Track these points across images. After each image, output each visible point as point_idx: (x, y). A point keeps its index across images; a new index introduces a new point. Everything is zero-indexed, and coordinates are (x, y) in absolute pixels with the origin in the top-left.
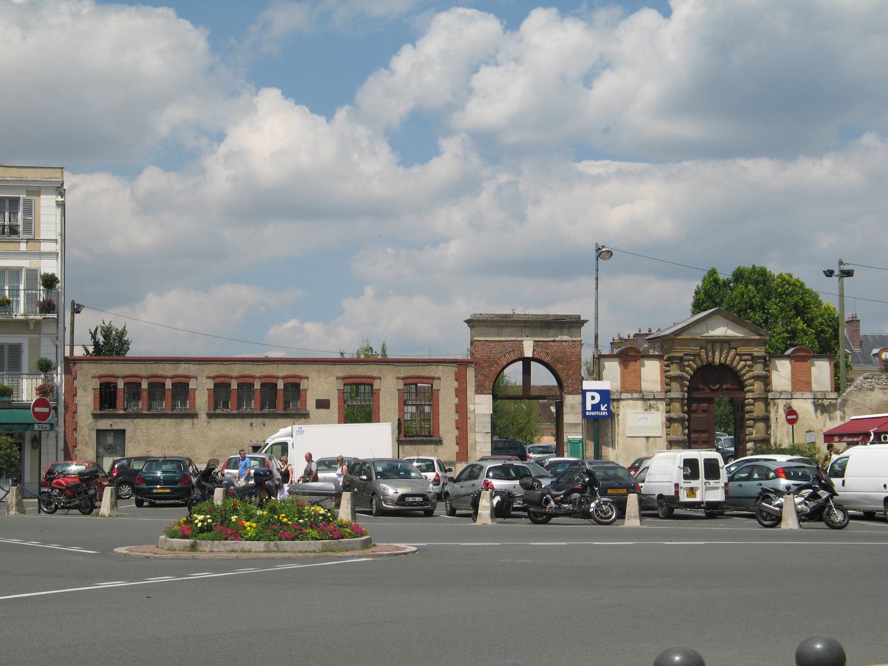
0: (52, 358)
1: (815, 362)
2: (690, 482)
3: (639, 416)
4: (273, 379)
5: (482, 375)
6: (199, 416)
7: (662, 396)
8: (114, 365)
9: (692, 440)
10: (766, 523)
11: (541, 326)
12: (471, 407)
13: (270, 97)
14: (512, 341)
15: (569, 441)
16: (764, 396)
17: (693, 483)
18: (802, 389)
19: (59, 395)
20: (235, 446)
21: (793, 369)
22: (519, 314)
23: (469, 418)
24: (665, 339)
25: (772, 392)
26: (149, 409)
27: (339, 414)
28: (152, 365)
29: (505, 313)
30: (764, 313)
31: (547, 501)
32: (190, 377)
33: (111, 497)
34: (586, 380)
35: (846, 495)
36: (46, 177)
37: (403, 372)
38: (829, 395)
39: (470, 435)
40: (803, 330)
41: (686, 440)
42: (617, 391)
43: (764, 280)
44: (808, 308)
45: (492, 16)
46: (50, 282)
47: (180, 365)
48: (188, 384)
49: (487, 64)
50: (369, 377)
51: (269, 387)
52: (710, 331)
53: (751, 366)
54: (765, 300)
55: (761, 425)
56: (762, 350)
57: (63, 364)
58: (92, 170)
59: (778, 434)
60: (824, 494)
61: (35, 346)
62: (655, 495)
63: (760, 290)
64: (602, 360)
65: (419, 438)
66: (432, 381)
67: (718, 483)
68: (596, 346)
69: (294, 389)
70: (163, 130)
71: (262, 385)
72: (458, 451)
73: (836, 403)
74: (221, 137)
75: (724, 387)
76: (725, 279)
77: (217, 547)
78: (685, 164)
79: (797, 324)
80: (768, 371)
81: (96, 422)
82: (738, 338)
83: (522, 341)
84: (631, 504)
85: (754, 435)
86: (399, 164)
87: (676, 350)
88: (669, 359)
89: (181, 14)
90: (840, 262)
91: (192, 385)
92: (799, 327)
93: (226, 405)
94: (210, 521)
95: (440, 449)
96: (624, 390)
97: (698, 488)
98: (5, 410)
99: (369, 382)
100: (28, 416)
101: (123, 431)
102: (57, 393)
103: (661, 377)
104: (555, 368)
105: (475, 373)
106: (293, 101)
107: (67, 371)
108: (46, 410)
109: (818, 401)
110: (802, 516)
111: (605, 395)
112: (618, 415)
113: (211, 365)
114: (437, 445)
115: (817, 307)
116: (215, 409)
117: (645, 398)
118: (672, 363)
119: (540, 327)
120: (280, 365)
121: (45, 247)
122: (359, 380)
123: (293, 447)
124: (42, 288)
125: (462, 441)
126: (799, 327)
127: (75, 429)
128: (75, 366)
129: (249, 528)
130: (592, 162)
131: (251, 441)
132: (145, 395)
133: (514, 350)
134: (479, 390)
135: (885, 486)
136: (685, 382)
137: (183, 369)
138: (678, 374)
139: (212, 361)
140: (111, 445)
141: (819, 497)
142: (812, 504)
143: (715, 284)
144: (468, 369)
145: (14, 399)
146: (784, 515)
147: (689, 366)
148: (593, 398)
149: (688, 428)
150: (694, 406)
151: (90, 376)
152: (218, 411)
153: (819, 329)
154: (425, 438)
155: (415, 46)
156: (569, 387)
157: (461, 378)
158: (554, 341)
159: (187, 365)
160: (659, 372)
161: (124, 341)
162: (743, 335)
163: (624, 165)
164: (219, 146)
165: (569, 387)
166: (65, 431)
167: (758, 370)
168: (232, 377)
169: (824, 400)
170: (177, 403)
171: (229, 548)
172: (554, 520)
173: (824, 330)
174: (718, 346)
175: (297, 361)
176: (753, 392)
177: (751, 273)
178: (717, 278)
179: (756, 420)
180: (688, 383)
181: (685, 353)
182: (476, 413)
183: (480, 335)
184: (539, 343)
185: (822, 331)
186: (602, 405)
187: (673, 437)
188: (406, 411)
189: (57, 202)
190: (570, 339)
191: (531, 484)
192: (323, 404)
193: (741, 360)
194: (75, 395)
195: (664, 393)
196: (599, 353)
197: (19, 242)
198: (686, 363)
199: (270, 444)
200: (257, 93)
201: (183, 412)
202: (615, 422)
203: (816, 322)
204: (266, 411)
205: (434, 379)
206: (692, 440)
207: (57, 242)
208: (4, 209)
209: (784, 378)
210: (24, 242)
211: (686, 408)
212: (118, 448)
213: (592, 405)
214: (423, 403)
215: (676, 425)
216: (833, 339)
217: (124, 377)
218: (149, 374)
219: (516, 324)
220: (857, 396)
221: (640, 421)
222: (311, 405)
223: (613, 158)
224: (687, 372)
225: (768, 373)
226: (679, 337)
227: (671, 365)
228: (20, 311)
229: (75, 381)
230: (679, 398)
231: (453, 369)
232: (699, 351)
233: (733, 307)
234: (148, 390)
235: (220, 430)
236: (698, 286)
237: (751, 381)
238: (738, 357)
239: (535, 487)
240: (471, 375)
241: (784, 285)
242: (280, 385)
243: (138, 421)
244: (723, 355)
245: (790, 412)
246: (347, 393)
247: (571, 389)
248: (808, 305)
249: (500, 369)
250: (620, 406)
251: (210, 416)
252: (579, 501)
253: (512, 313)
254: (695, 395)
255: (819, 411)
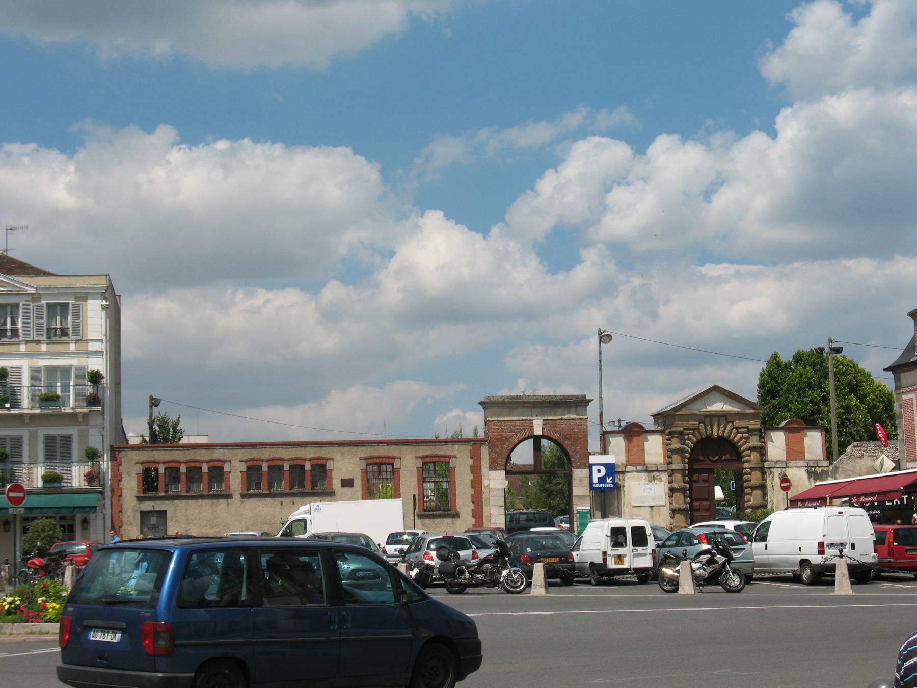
0: (98, 446)
1: (808, 433)
2: (618, 550)
3: (644, 487)
4: (301, 461)
5: (495, 452)
6: (234, 497)
7: (664, 467)
8: (155, 452)
9: (694, 508)
10: (665, 588)
11: (549, 406)
12: (485, 482)
13: (434, 219)
14: (522, 420)
15: (578, 512)
16: (761, 465)
17: (621, 551)
18: (796, 458)
19: (106, 480)
20: (267, 524)
21: (787, 439)
22: (528, 396)
23: (484, 493)
24: (666, 415)
25: (768, 461)
26: (188, 491)
27: (363, 492)
28: (189, 451)
29: (516, 395)
30: (821, 391)
31: (461, 572)
32: (224, 461)
33: (72, 576)
34: (594, 455)
35: (768, 558)
36: (92, 284)
37: (421, 451)
38: (820, 463)
39: (485, 508)
40: (856, 405)
41: (687, 508)
42: (622, 464)
43: (821, 362)
44: (860, 386)
45: (623, 143)
46: (95, 378)
47: (216, 451)
48: (222, 468)
49: (619, 184)
50: (389, 457)
51: (297, 468)
52: (708, 407)
53: (747, 438)
54: (822, 380)
55: (758, 493)
56: (757, 423)
57: (109, 452)
58: (283, 287)
59: (775, 501)
60: (721, 559)
61: (84, 436)
62: (587, 562)
63: (817, 370)
64: (607, 436)
65: (438, 512)
66: (448, 459)
67: (646, 549)
68: (601, 423)
69: (321, 470)
70: (343, 250)
71: (165, 469)
72: (474, 523)
73: (828, 470)
74: (391, 254)
75: (723, 458)
76: (786, 362)
77: (17, 629)
78: (796, 265)
79: (850, 400)
80: (764, 442)
81: (140, 504)
82: (734, 412)
83: (532, 420)
84: (537, 573)
85: (752, 502)
86: (546, 273)
87: (677, 425)
88: (670, 433)
89: (356, 152)
90: (830, 340)
91: (227, 468)
92: (853, 403)
93: (258, 486)
94: (18, 603)
95: (458, 522)
96: (629, 463)
97: (625, 556)
98: (55, 495)
99: (389, 461)
100: (77, 500)
101: (165, 512)
102: (104, 479)
103: (664, 450)
104: (564, 445)
105: (489, 450)
106: (454, 221)
107: (113, 458)
108: (21, 495)
109: (811, 469)
110: (700, 581)
111: (611, 469)
112: (624, 486)
113: (243, 450)
114: (454, 518)
115: (869, 385)
116: (248, 490)
117: (650, 471)
118: (673, 437)
119: (548, 407)
120: (307, 448)
121: (92, 347)
122: (381, 460)
123: (311, 524)
124: (89, 384)
125: (478, 514)
126: (853, 403)
127: (121, 511)
128: (120, 454)
129: (51, 610)
130: (714, 266)
131: (281, 519)
132: (183, 478)
133: (524, 429)
134: (493, 466)
135: (800, 549)
136: (686, 454)
137: (218, 454)
138: (679, 447)
139: (244, 446)
140: (154, 525)
141: (716, 562)
142: (709, 569)
143: (778, 366)
144: (482, 447)
145: (65, 485)
146: (681, 580)
147: (689, 439)
148: (599, 471)
149: (690, 497)
150: (695, 476)
151: (134, 462)
152: (251, 492)
153: (871, 404)
154: (442, 512)
155: (557, 171)
156: (576, 462)
157: (475, 456)
158: (561, 419)
159: (221, 450)
160: (662, 446)
161: (177, 430)
162: (739, 410)
163: (742, 268)
164: (390, 262)
165: (576, 462)
166: (111, 513)
167: (754, 441)
168: (263, 460)
169: (817, 468)
170: (213, 485)
171: (28, 630)
172: (468, 590)
173: (876, 405)
174: (715, 420)
175: (323, 444)
176: (750, 462)
177: (809, 356)
178: (779, 361)
179: (753, 488)
180: (688, 455)
181: (685, 427)
182: (490, 487)
183: (492, 416)
184: (548, 422)
185: (874, 407)
186: (607, 478)
187: (675, 506)
188: (425, 488)
189: (102, 305)
190: (577, 417)
191: (447, 555)
192: (347, 483)
193: (738, 433)
194: (120, 480)
195: (666, 465)
196: (604, 430)
197: (69, 343)
198: (686, 437)
199: (290, 521)
200: (422, 215)
201: (218, 493)
202: (620, 493)
203: (868, 398)
204: (295, 490)
205: (450, 457)
206: (694, 508)
207: (102, 342)
208: (56, 314)
209: (779, 448)
210: (73, 343)
211: (687, 478)
212: (161, 528)
213: (598, 478)
214: (441, 480)
215: (678, 494)
216: (884, 413)
217: (164, 463)
218: (187, 459)
219: (526, 405)
220: (847, 464)
221: (644, 491)
222: (336, 483)
223: (732, 261)
224: (687, 445)
225: (764, 444)
226: (678, 413)
227: (672, 439)
228: (71, 404)
229: (120, 467)
230: (681, 470)
231: (468, 448)
232: (698, 425)
233: (793, 386)
234: (186, 474)
235: (253, 509)
236: (763, 369)
237: (747, 452)
238: (735, 430)
239: (451, 558)
240: (485, 453)
241: (838, 366)
242: (308, 467)
243: (177, 502)
244: (721, 429)
245: (785, 479)
246: (370, 472)
247: (579, 463)
248: (860, 383)
249: (511, 446)
250: (625, 478)
251: (243, 496)
252: (490, 572)
253: (522, 394)
254: (696, 466)
255: (812, 478)
